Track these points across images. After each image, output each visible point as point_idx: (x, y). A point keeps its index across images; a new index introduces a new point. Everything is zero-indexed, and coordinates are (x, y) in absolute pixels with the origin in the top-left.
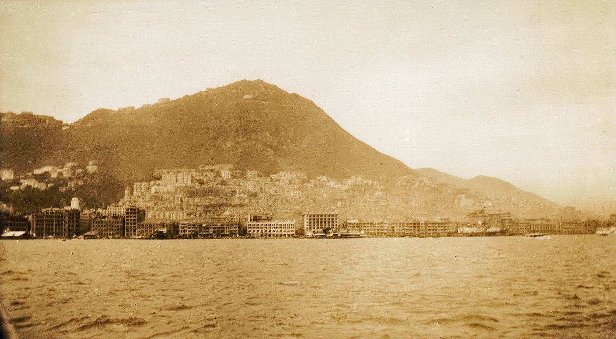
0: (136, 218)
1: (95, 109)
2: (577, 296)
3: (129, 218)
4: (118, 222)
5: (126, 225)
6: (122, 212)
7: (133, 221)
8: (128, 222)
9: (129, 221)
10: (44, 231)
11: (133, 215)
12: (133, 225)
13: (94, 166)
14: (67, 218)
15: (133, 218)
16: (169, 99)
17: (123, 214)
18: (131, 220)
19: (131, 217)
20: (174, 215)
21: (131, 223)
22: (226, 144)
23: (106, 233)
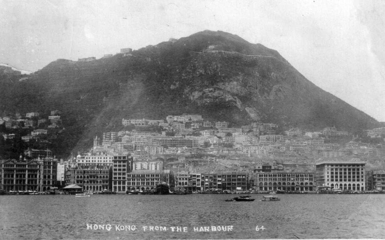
0: (126, 168)
1: (54, 59)
2: (338, 228)
3: (118, 168)
4: (104, 172)
5: (113, 176)
6: (108, 162)
7: (122, 172)
8: (115, 172)
9: (117, 172)
10: (51, 178)
11: (122, 164)
12: (122, 176)
13: (57, 116)
14: (42, 167)
15: (122, 168)
16: (131, 49)
17: (110, 164)
18: (120, 170)
19: (120, 166)
20: (154, 166)
21: (120, 174)
22: (193, 94)
23: (96, 186)
